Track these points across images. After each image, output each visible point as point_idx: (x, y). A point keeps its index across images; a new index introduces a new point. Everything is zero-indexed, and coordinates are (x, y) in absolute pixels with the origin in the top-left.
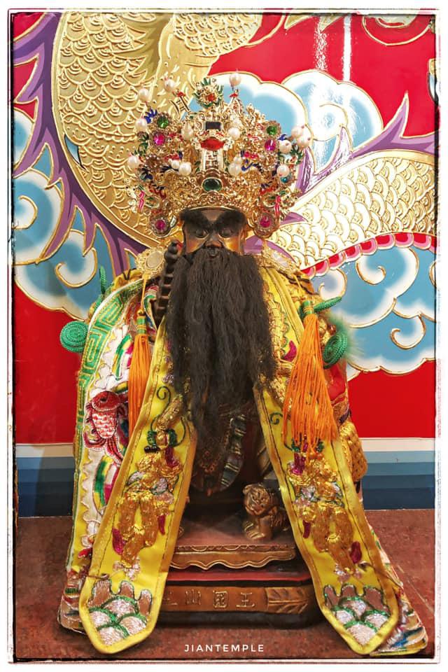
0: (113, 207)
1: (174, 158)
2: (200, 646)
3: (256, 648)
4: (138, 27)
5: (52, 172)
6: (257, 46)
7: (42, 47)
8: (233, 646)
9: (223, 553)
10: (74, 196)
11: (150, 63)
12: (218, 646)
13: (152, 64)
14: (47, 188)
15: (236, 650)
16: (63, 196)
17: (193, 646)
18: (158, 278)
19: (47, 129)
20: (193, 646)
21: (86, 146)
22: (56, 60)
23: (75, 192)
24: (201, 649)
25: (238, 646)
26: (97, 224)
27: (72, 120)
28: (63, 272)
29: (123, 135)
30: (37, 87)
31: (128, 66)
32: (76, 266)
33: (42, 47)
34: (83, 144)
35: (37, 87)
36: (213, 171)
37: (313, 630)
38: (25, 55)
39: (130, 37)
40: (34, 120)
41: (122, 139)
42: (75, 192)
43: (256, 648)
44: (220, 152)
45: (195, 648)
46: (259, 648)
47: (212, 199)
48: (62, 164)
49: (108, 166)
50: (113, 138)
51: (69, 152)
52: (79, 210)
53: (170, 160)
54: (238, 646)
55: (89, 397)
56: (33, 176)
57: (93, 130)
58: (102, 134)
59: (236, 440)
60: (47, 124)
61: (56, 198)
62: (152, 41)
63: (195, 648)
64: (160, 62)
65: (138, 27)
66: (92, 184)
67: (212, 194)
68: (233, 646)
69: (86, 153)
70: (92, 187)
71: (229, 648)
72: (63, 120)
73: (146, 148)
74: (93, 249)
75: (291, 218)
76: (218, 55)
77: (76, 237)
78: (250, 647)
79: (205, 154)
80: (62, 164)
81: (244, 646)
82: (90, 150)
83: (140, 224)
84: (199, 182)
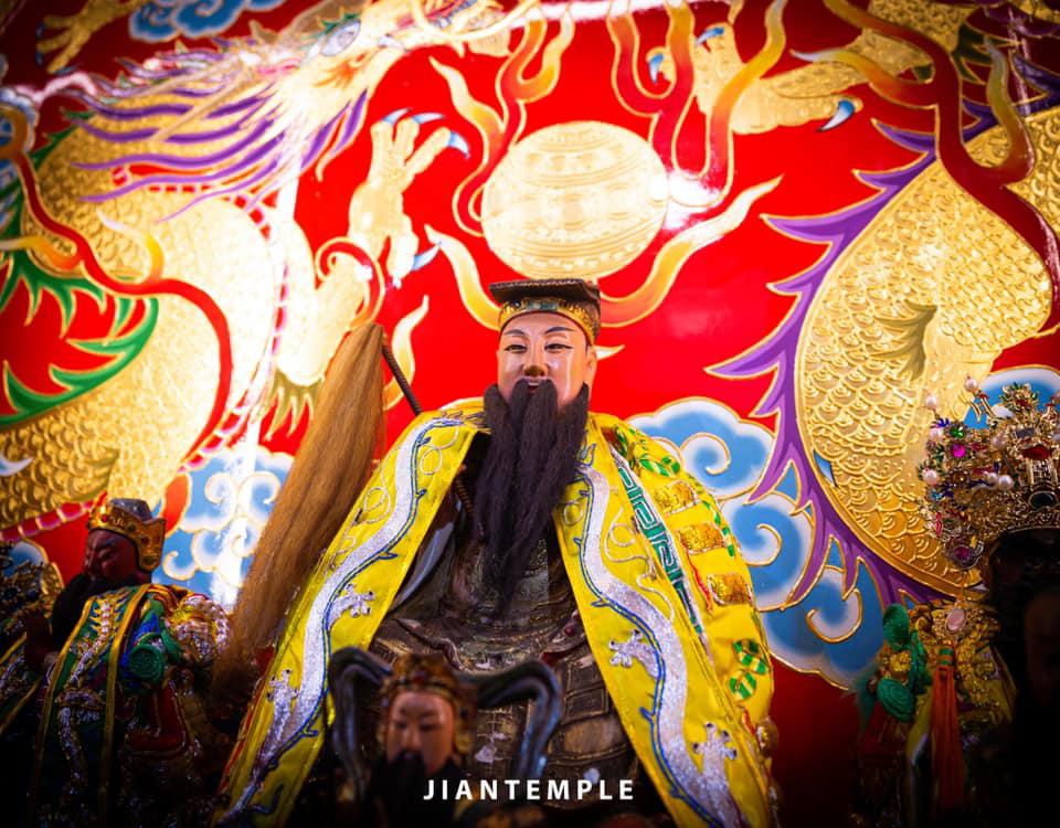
0: (881, 536)
1: (989, 470)
4: (894, 325)
5: (799, 495)
6: (1049, 336)
7: (782, 355)
10: (828, 523)
11: (914, 363)
13: (917, 364)
14: (794, 515)
16: (814, 524)
17: (445, 783)
19: (791, 445)
20: (445, 783)
21: (841, 461)
22: (799, 368)
23: (828, 517)
24: (468, 793)
26: (859, 558)
27: (822, 432)
28: (816, 620)
29: (887, 446)
30: (778, 398)
31: (888, 368)
32: (835, 613)
33: (782, 355)
34: (837, 460)
35: (778, 398)
36: (1043, 484)
38: (762, 364)
39: (887, 341)
40: (776, 434)
41: (887, 452)
42: (828, 517)
44: (1050, 461)
45: (453, 790)
47: (1045, 518)
48: (812, 486)
49: (870, 485)
50: (875, 451)
51: (820, 471)
52: (833, 539)
53: (986, 472)
56: (777, 500)
57: (849, 442)
58: (861, 446)
60: (791, 440)
61: (806, 525)
62: (915, 339)
64: (927, 362)
65: (894, 325)
66: (851, 508)
67: (1045, 511)
69: (841, 470)
70: (851, 511)
72: (810, 433)
73: (941, 461)
74: (856, 590)
77: (833, 575)
79: (1031, 465)
80: (812, 486)
82: (846, 467)
83: (919, 556)
84: (1025, 497)
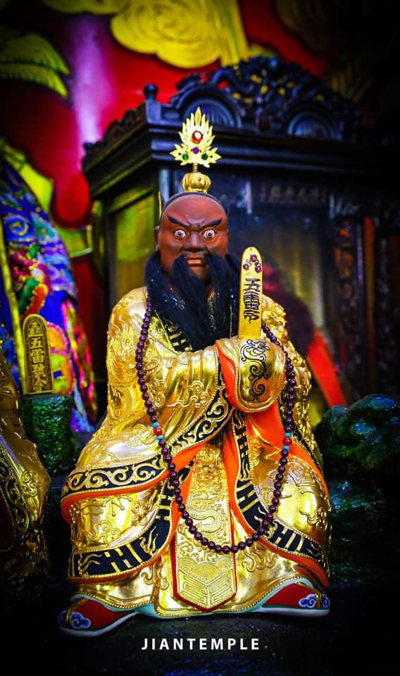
2: (164, 640)
3: (247, 643)
8: (214, 641)
9: (110, 489)
12: (191, 640)
15: (217, 648)
17: (154, 640)
18: (171, 451)
20: (154, 640)
25: (221, 640)
37: (31, 78)
43: (247, 643)
45: (158, 645)
46: (253, 644)
54: (221, 640)
55: (179, 610)
59: (199, 277)
63: (158, 645)
68: (214, 641)
71: (209, 643)
75: (158, 448)
76: (148, 552)
78: (238, 643)
81: (229, 640)
